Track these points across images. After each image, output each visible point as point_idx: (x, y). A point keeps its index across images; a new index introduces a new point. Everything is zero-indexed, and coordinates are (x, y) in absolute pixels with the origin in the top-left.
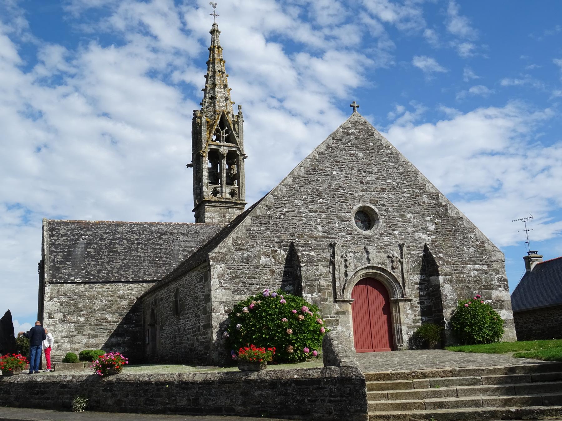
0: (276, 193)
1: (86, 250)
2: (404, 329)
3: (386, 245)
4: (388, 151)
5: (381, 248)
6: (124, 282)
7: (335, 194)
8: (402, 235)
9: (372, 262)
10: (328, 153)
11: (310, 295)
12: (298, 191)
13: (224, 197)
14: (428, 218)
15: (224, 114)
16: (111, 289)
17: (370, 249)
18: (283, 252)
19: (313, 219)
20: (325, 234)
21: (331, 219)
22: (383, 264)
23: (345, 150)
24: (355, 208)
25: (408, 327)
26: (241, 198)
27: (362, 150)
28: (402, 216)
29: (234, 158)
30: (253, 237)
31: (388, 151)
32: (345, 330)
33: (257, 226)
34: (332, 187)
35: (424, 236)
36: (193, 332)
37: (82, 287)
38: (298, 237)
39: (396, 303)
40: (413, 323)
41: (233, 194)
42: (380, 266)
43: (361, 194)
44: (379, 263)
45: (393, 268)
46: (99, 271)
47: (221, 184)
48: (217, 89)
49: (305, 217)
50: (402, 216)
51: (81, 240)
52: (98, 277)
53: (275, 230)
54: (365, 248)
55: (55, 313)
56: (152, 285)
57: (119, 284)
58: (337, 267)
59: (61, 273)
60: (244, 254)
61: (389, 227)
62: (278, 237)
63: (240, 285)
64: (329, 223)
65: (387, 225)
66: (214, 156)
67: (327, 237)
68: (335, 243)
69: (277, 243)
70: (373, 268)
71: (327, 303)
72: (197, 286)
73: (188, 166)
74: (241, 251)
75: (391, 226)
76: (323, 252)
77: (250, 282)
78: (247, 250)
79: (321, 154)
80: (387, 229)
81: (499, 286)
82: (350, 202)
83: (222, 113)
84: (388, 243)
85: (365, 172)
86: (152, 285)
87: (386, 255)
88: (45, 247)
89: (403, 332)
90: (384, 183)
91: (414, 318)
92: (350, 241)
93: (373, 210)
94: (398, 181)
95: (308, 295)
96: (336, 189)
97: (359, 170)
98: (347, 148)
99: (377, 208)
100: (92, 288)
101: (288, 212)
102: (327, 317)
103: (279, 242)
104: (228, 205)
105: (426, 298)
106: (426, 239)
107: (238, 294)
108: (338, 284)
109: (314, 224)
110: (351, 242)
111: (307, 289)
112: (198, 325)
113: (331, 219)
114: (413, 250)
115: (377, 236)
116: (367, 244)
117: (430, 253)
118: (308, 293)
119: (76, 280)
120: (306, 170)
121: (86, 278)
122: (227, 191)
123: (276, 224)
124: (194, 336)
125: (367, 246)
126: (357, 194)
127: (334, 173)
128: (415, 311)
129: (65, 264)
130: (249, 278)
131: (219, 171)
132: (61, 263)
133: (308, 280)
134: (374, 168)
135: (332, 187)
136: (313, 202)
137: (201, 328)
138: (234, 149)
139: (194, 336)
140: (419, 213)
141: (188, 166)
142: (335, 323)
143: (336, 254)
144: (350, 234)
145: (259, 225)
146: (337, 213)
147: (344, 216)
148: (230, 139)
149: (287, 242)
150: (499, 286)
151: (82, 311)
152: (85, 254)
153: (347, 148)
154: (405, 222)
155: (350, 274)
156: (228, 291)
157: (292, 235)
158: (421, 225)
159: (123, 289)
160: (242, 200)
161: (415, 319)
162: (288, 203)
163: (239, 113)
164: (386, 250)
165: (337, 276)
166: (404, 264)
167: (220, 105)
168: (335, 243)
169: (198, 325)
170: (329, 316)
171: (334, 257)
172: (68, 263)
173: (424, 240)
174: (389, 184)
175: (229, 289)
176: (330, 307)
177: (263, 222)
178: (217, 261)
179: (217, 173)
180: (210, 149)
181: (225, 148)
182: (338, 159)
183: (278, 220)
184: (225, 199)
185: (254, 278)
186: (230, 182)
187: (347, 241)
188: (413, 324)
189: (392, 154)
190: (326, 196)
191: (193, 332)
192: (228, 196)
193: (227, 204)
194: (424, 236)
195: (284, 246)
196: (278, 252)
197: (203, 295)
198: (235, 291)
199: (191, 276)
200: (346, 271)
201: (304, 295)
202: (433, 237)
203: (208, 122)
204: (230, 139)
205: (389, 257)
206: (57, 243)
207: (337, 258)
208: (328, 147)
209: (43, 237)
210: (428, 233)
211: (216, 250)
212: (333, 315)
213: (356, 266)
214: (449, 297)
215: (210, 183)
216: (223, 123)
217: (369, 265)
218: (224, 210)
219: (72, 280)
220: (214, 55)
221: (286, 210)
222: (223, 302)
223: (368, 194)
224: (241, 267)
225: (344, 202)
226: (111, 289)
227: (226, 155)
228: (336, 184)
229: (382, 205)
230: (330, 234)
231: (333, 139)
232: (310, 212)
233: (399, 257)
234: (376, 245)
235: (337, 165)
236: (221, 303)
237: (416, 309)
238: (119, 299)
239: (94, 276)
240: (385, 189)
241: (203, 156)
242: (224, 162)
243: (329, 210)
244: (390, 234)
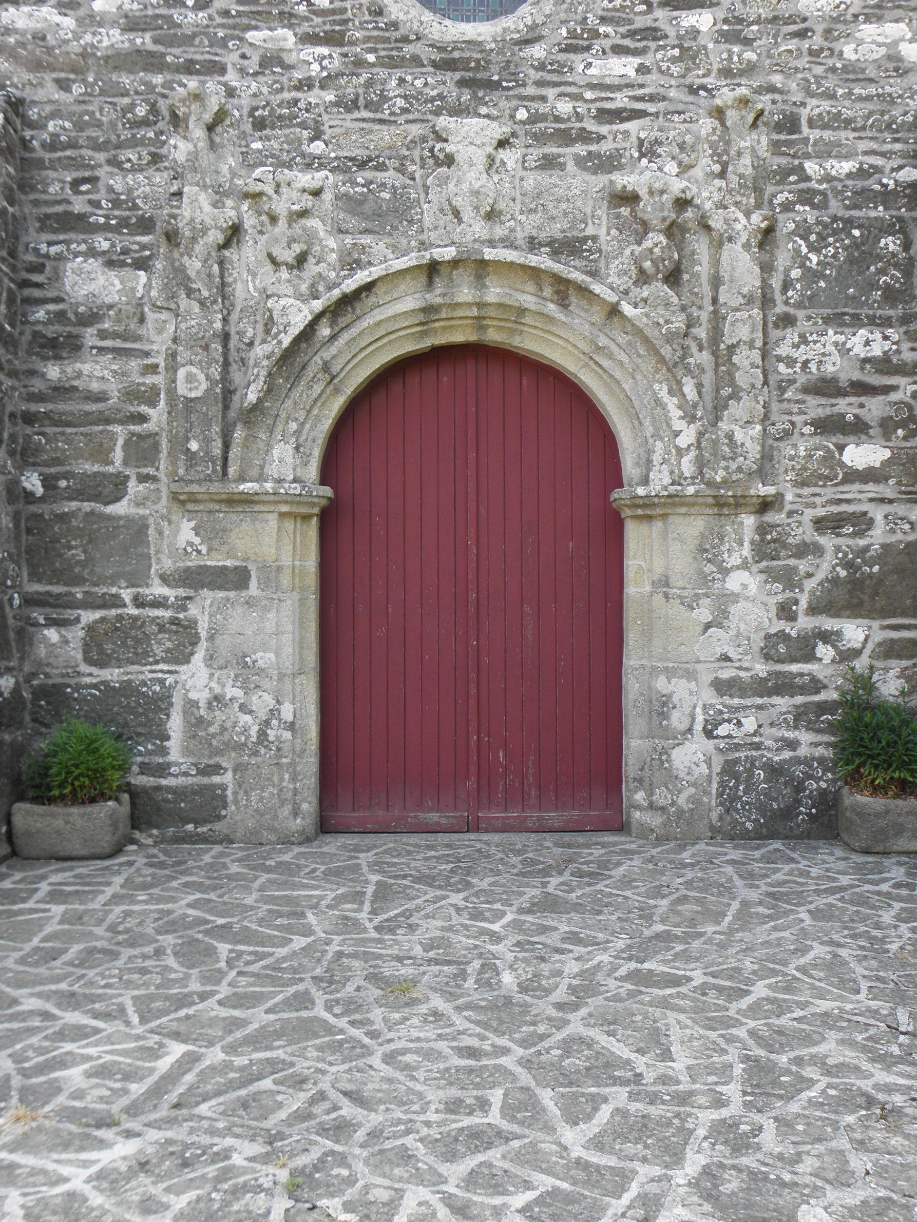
5: (566, 138)
8: (747, 42)
22: (568, 247)
25: (722, 687)
32: (231, 692)
40: (767, 657)
42: (542, 260)
44: (533, 244)
71: (121, 508)
76: (114, 162)
81: (304, 214)
84: (621, 100)
102: (116, 602)
105: (888, 490)
110: (330, 97)
114: (826, 152)
115: (538, 52)
128: (789, 579)
142: (161, 645)
150: (304, 214)
161: (783, 636)
164: (605, 147)
170: (127, 595)
176: (139, 529)
187: (306, 84)
188: (761, 669)
212: (158, 589)
230: (170, 42)
234: (522, 114)
237: (803, 566)
244: (652, 33)
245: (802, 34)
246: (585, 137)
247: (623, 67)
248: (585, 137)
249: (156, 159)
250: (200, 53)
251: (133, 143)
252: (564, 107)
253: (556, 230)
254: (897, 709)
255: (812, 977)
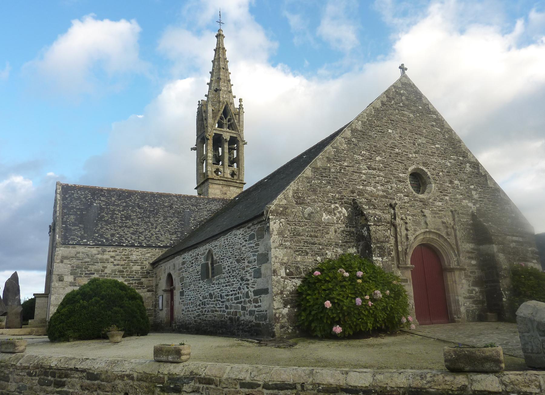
0: (335, 145)
1: (99, 214)
2: (461, 300)
3: (440, 211)
4: (435, 116)
5: (436, 213)
6: (137, 247)
7: (391, 153)
9: (429, 226)
10: (383, 110)
11: (380, 259)
12: (356, 145)
13: (225, 176)
14: (472, 187)
15: (227, 104)
16: (123, 253)
17: (427, 212)
18: (344, 211)
19: (372, 176)
20: (385, 194)
21: (389, 178)
23: (398, 110)
24: (410, 169)
26: (240, 178)
27: (413, 112)
28: (451, 182)
29: (235, 142)
30: (314, 191)
31: (435, 116)
33: (318, 179)
34: (388, 145)
35: (470, 204)
36: (237, 298)
37: (94, 251)
38: (358, 195)
39: (451, 272)
41: (233, 174)
43: (414, 155)
45: (448, 234)
46: (113, 235)
47: (223, 165)
48: (221, 83)
49: (364, 174)
50: (451, 182)
51: (95, 204)
52: (112, 240)
53: (336, 184)
54: (422, 212)
55: (65, 275)
56: (165, 250)
57: (132, 249)
58: (398, 230)
59: (74, 235)
60: (305, 209)
61: (441, 192)
62: (339, 193)
63: (302, 244)
64: (387, 182)
65: (439, 189)
66: (218, 141)
67: (386, 197)
68: (396, 204)
69: (338, 199)
70: (430, 232)
72: (245, 246)
73: (192, 149)
74: (303, 206)
75: (442, 191)
77: (312, 241)
78: (308, 205)
79: (377, 110)
80: (439, 194)
82: (405, 162)
83: (225, 103)
84: (440, 208)
85: (417, 134)
86: (165, 250)
87: (440, 220)
88: (58, 209)
89: (460, 303)
90: (434, 147)
91: (469, 288)
92: (408, 203)
93: (426, 174)
94: (445, 146)
95: (378, 258)
96: (393, 148)
97: (411, 131)
98: (400, 108)
99: (430, 171)
100: (104, 251)
101: (347, 166)
103: (341, 199)
104: (229, 183)
106: (473, 207)
107: (299, 255)
108: (400, 248)
109: (373, 182)
111: (377, 251)
112: (246, 290)
113: (389, 178)
114: (463, 218)
115: (431, 200)
116: (423, 208)
117: (480, 221)
118: (378, 257)
119: (88, 243)
120: (364, 123)
121: (99, 241)
122: (228, 172)
123: (337, 178)
124: (237, 303)
125: (423, 210)
126: (411, 156)
127: (390, 131)
129: (78, 226)
130: (311, 236)
131: (220, 154)
132: (74, 225)
133: (378, 241)
134: (424, 131)
135: (388, 145)
136: (371, 159)
137: (251, 294)
138: (235, 136)
139: (237, 303)
140: (464, 181)
141: (192, 149)
143: (397, 216)
144: (407, 196)
145: (320, 177)
146: (394, 173)
147: (401, 177)
148: (232, 126)
149: (348, 199)
151: (94, 274)
152: (98, 217)
153: (400, 108)
154: (453, 188)
155: (411, 238)
156: (289, 251)
157: (353, 192)
158: (467, 192)
159: (136, 254)
160: (241, 180)
162: (348, 157)
163: (240, 105)
164: (440, 215)
165: (399, 239)
166: (457, 231)
167: (223, 96)
168: (396, 204)
169: (246, 290)
171: (395, 219)
172: (81, 225)
173: (471, 207)
174: (437, 148)
175: (290, 248)
177: (324, 175)
178: (277, 214)
179: (219, 156)
180: (215, 133)
181: (228, 134)
182: (393, 117)
183: (339, 174)
184: (226, 178)
185: (316, 237)
186: (232, 162)
187: (405, 203)
189: (438, 119)
190: (383, 154)
191: (237, 298)
192: (229, 177)
193: (228, 183)
194: (470, 204)
195: (346, 203)
196: (340, 209)
197: (254, 255)
198: (297, 251)
199: (236, 235)
200: (407, 235)
201: (374, 258)
202: (478, 206)
203: (213, 110)
204: (232, 126)
205: (443, 223)
206: (70, 206)
207: (398, 221)
208: (383, 104)
209: (56, 200)
210: (473, 201)
211: (275, 202)
213: (415, 230)
214: (504, 267)
215: (213, 164)
216: (226, 112)
217: (428, 230)
218: (225, 188)
219: (84, 242)
220: (219, 55)
221: (346, 164)
222: (285, 263)
223: (420, 156)
224: (303, 224)
225: (399, 162)
226: (123, 253)
227: (228, 139)
228: (392, 143)
229: (433, 169)
231: (387, 97)
232: (369, 169)
233: (452, 223)
235: (392, 124)
236: (282, 264)
238: (132, 264)
239: (107, 240)
240: (435, 153)
241: (208, 139)
242: (226, 146)
243: (387, 169)
244: (442, 199)
245: (458, 201)
246: (438, 214)
247: (440, 204)
248: (438, 214)
249: (389, 212)
250: (391, 196)
251: (386, 210)
252: (435, 209)
253: (436, 227)
254: (352, 213)
255: (515, 242)
